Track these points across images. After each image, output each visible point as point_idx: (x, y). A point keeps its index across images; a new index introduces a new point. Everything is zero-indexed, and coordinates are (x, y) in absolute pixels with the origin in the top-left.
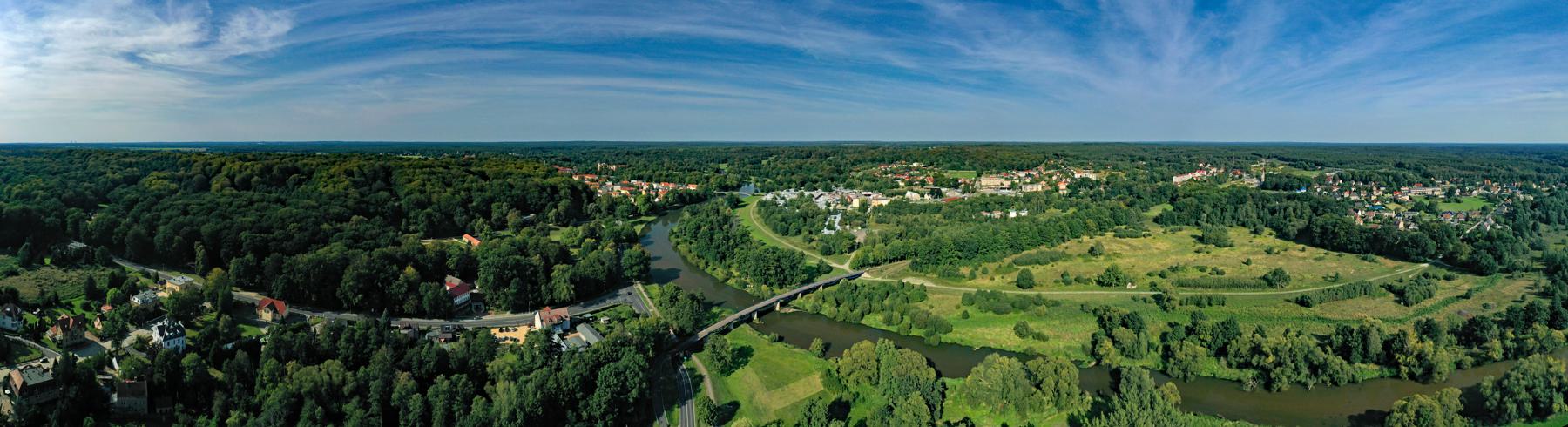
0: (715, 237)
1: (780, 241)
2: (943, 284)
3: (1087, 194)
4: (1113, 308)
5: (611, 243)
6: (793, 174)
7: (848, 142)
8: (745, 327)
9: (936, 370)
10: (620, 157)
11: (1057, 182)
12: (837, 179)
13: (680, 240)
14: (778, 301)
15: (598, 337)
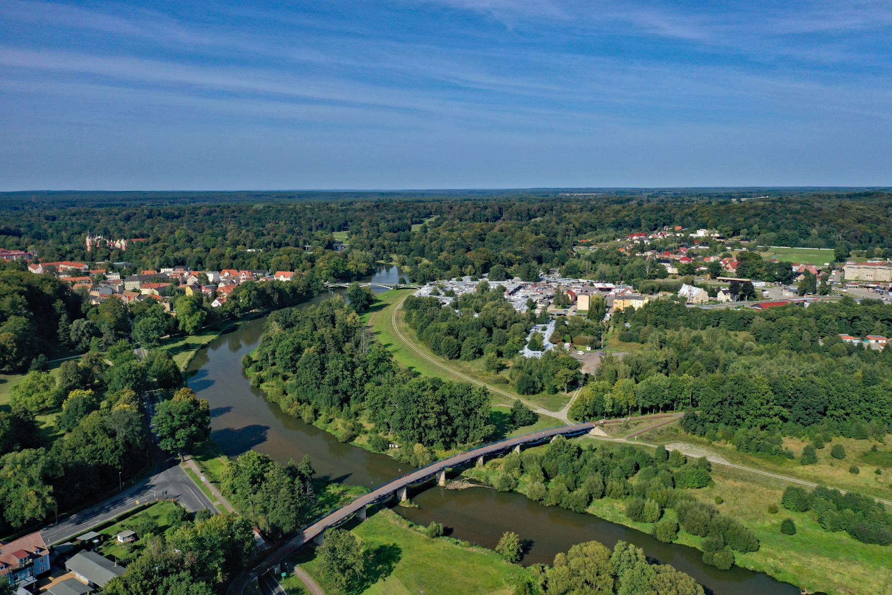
0: (330, 365)
1: (445, 367)
2: (744, 462)
5: (128, 393)
6: (468, 250)
7: (572, 191)
8: (387, 514)
10: (134, 222)
12: (550, 260)
13: (264, 374)
14: (443, 469)
15: (113, 570)
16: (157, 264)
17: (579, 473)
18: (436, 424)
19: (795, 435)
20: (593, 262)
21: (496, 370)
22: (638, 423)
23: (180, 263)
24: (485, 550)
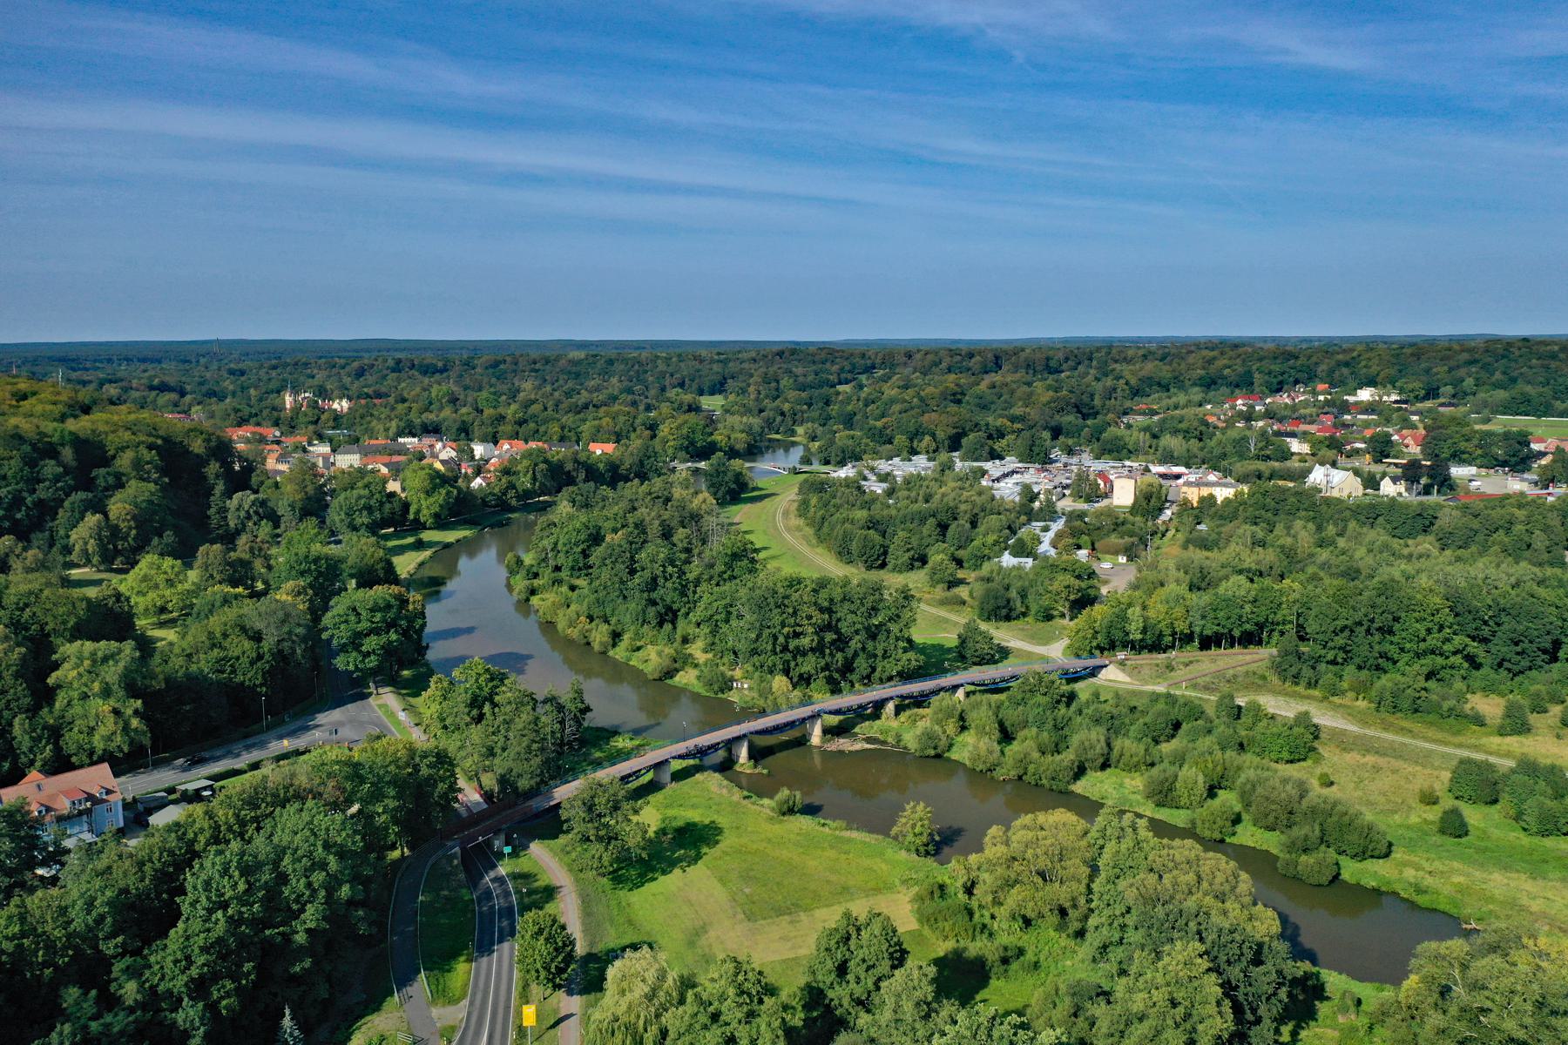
8: (711, 782)
10: (370, 378)
12: (1075, 432)
14: (815, 717)
16: (393, 430)
17: (1066, 729)
18: (814, 645)
19: (1493, 692)
20: (1155, 436)
21: (946, 585)
22: (1191, 662)
23: (433, 430)
24: (876, 836)
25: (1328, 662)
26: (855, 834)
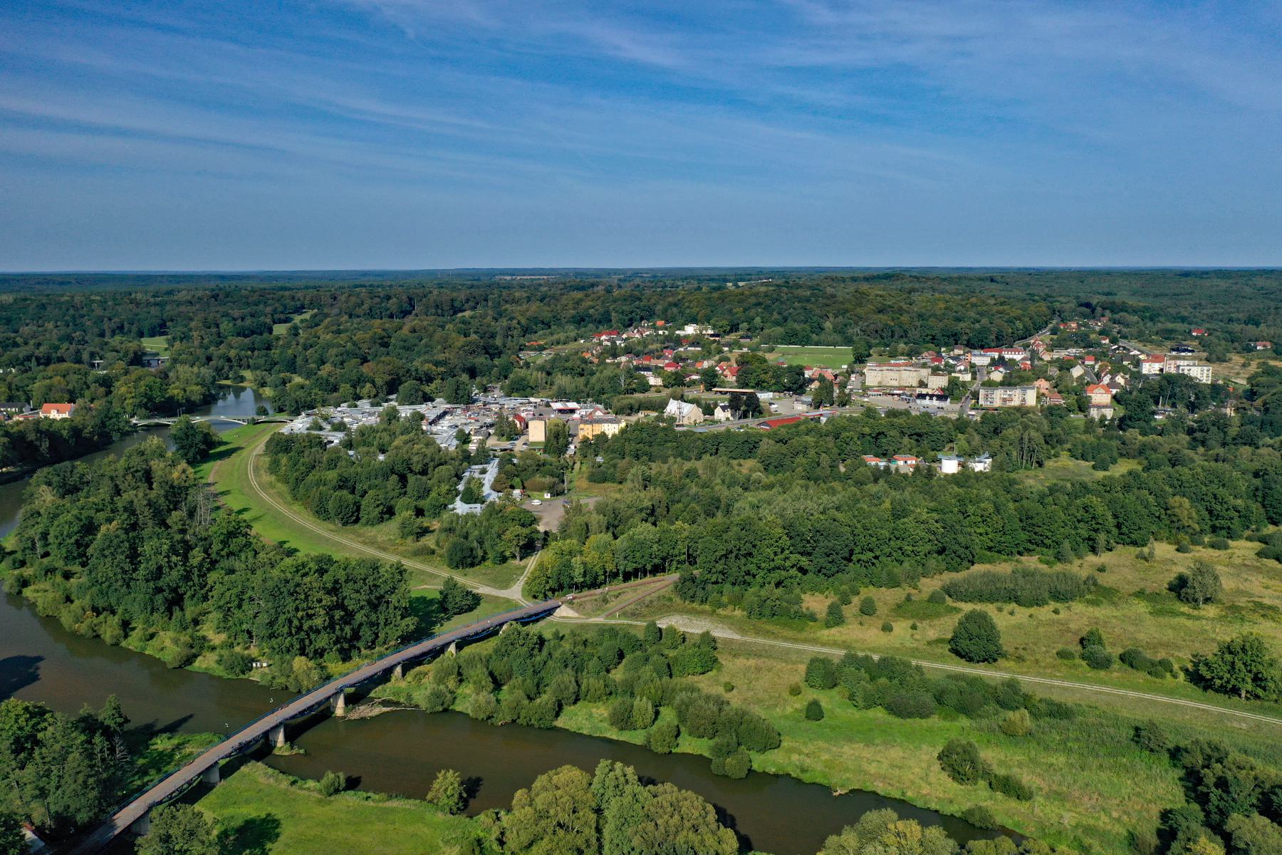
0: (146, 548)
1: (337, 538)
2: (758, 632)
3: (1176, 424)
4: (1235, 755)
7: (513, 272)
8: (255, 771)
9: (737, 833)
11: (1083, 384)
13: (27, 572)
17: (543, 672)
18: (326, 624)
20: (549, 374)
21: (414, 537)
22: (620, 594)
24: (412, 801)
25: (713, 583)
26: (394, 803)
